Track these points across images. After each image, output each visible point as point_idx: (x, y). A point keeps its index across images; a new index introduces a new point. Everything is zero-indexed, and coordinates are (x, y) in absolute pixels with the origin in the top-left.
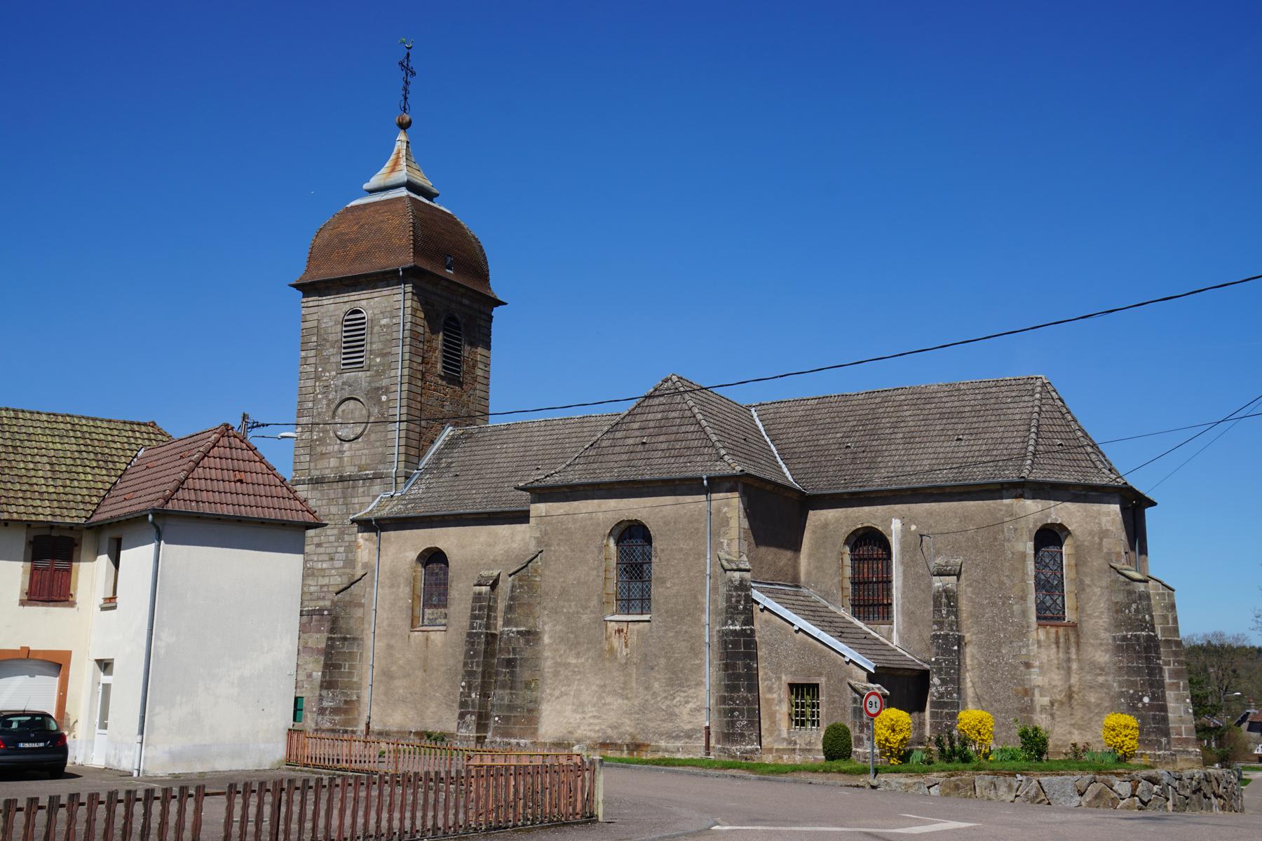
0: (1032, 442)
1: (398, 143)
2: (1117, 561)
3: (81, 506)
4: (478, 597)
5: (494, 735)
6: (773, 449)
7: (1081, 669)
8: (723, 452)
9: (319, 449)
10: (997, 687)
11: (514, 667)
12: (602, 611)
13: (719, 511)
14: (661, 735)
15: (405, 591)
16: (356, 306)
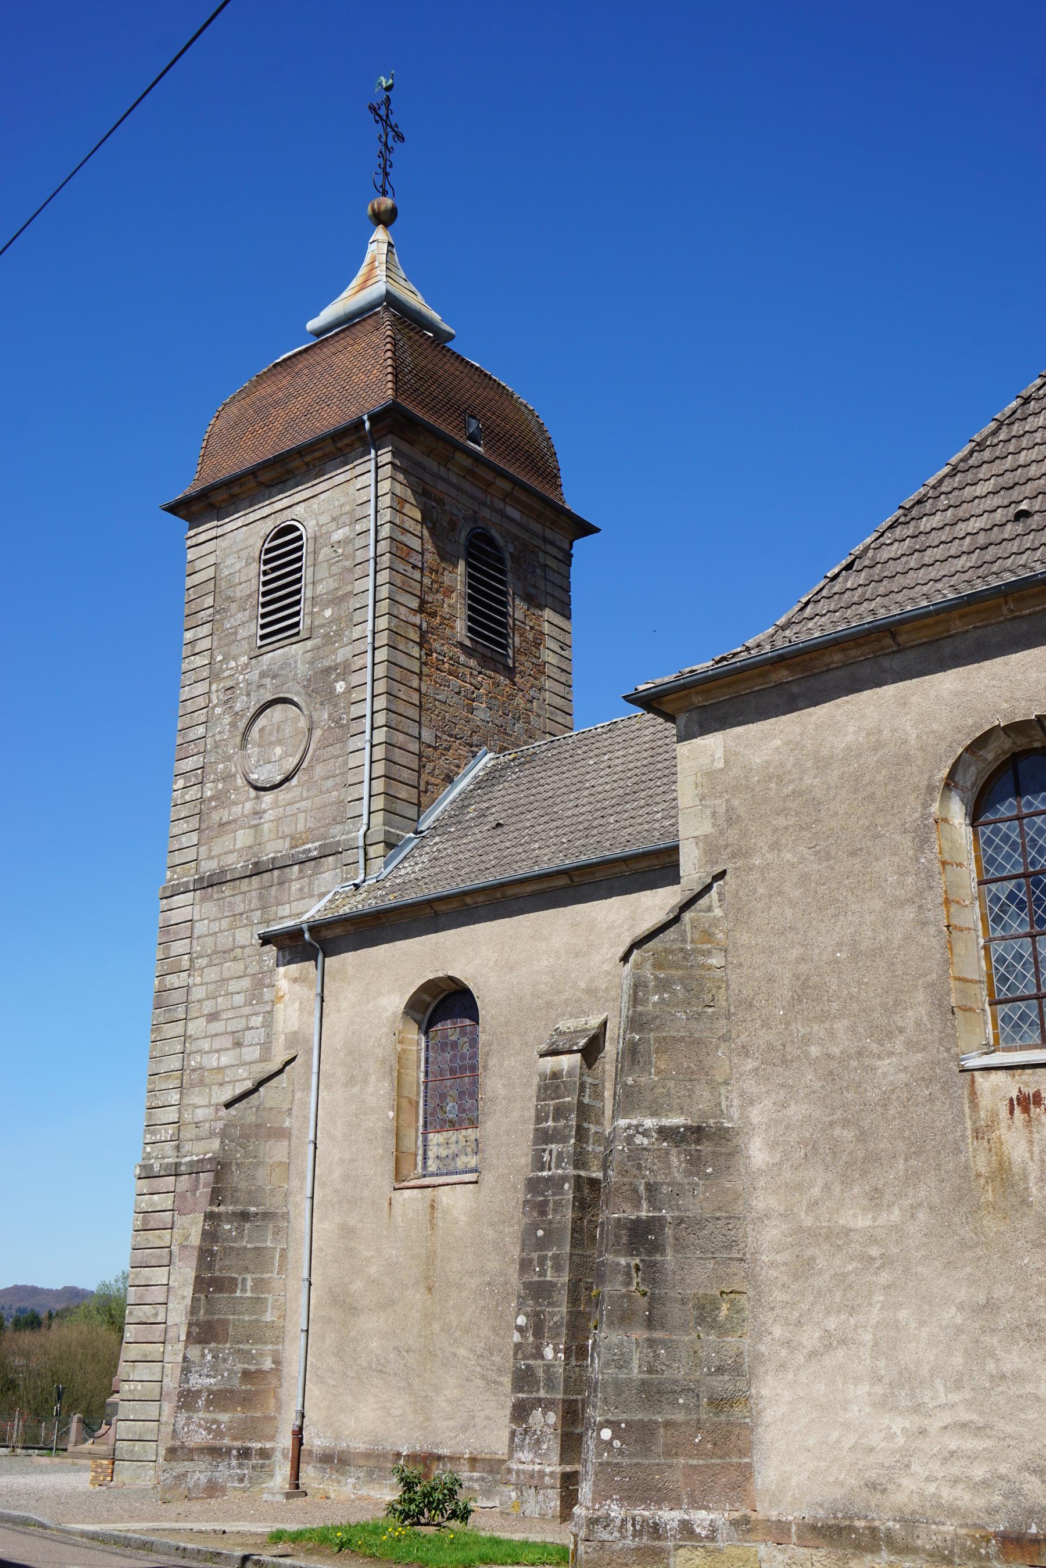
1: (372, 248)
4: (551, 1085)
5: (600, 1496)
9: (215, 817)
11: (657, 1247)
12: (949, 1039)
15: (378, 1091)
16: (283, 519)
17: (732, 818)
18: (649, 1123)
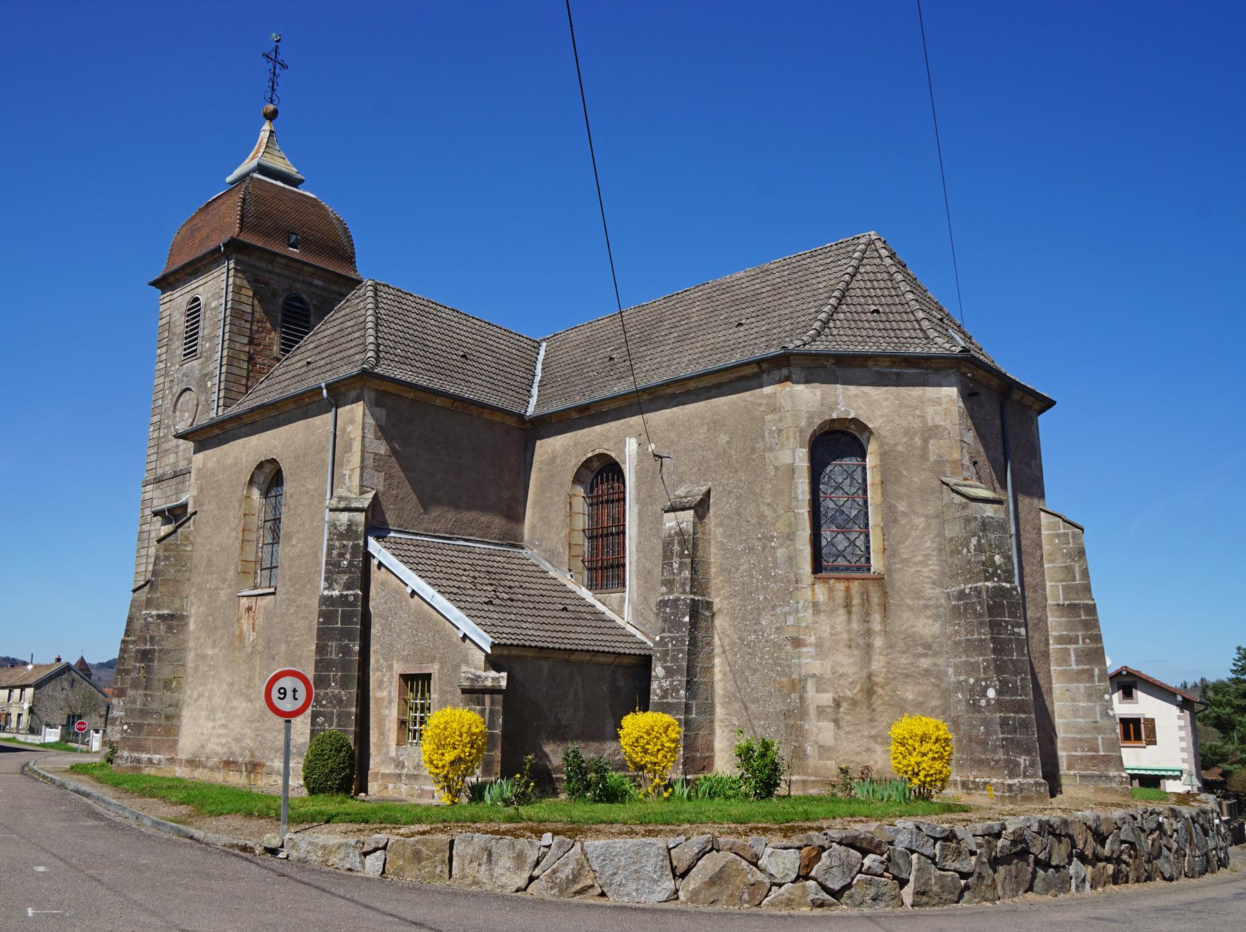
7: (890, 646)
10: (754, 679)
11: (152, 660)
13: (344, 432)
18: (154, 612)
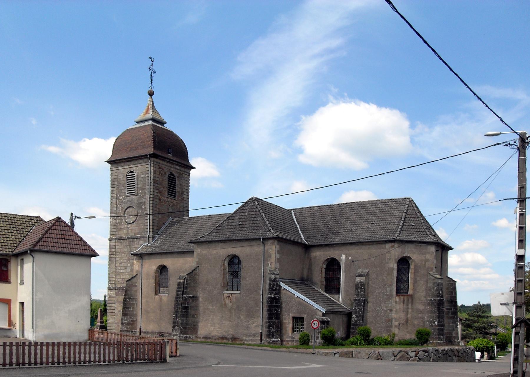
0: (401, 224)
2: (432, 271)
3: (10, 247)
4: (179, 284)
6: (298, 226)
7: (412, 311)
8: (270, 228)
10: (378, 318)
13: (267, 251)
14: (244, 335)
16: (132, 170)
17: (200, 259)
